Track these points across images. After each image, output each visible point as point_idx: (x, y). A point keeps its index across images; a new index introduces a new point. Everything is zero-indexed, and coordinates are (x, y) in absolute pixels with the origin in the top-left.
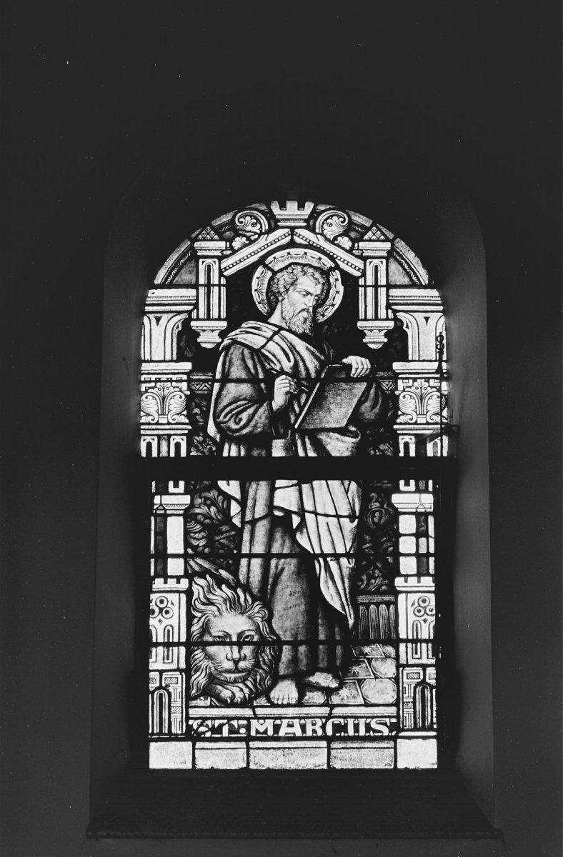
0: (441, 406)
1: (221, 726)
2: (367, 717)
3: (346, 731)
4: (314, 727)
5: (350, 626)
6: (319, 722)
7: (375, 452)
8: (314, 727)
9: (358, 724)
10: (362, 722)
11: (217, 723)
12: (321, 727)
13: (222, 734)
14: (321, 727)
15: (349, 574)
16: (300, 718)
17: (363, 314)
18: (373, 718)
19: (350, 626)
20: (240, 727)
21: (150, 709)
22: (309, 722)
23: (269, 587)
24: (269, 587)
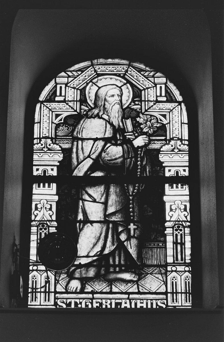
0: (168, 88)
1: (70, 303)
2: (135, 299)
3: (71, 306)
4: (106, 304)
5: (75, 267)
6: (109, 301)
7: (139, 151)
8: (106, 304)
9: (137, 303)
10: (154, 302)
11: (69, 301)
12: (109, 304)
13: (71, 307)
14: (109, 304)
15: (111, 227)
16: (141, 299)
17: (144, 98)
18: (159, 300)
19: (75, 267)
21: (190, 289)
22: (104, 301)
23: (21, 290)
24: (21, 290)
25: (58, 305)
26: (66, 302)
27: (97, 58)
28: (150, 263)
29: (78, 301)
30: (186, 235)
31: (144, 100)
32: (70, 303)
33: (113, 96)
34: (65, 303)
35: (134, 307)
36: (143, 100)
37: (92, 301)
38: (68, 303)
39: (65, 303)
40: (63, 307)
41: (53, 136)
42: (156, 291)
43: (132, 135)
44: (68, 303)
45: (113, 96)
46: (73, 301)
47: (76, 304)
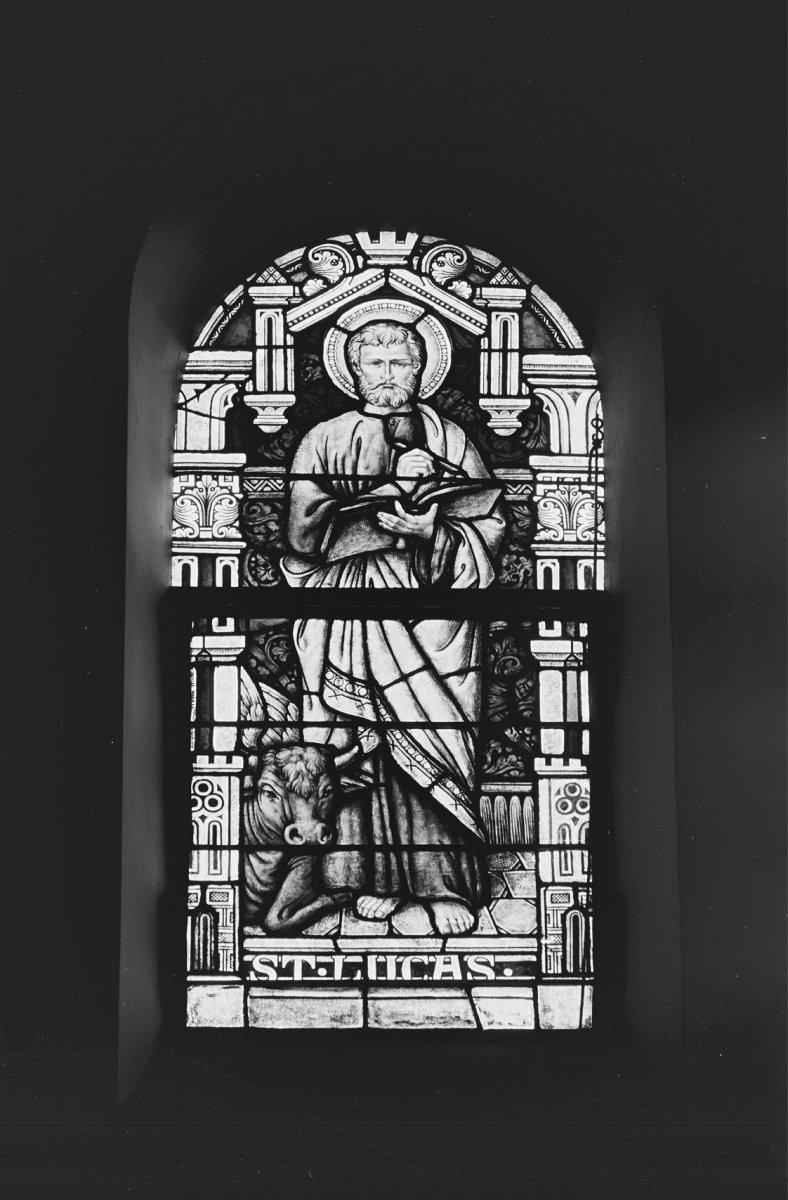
1: (291, 965)
11: (286, 960)
20: (319, 965)
25: (253, 970)
26: (280, 964)
27: (541, 1038)
28: (385, 837)
29: (311, 961)
30: (552, 855)
31: (486, 347)
32: (291, 965)
33: (378, 362)
34: (276, 965)
35: (558, 588)
36: (482, 392)
37: (365, 960)
38: (284, 966)
39: (276, 965)
40: (267, 976)
41: (568, 969)
42: (261, 427)
43: (419, 241)
44: (284, 966)
45: (378, 362)
46: (298, 961)
47: (306, 965)
